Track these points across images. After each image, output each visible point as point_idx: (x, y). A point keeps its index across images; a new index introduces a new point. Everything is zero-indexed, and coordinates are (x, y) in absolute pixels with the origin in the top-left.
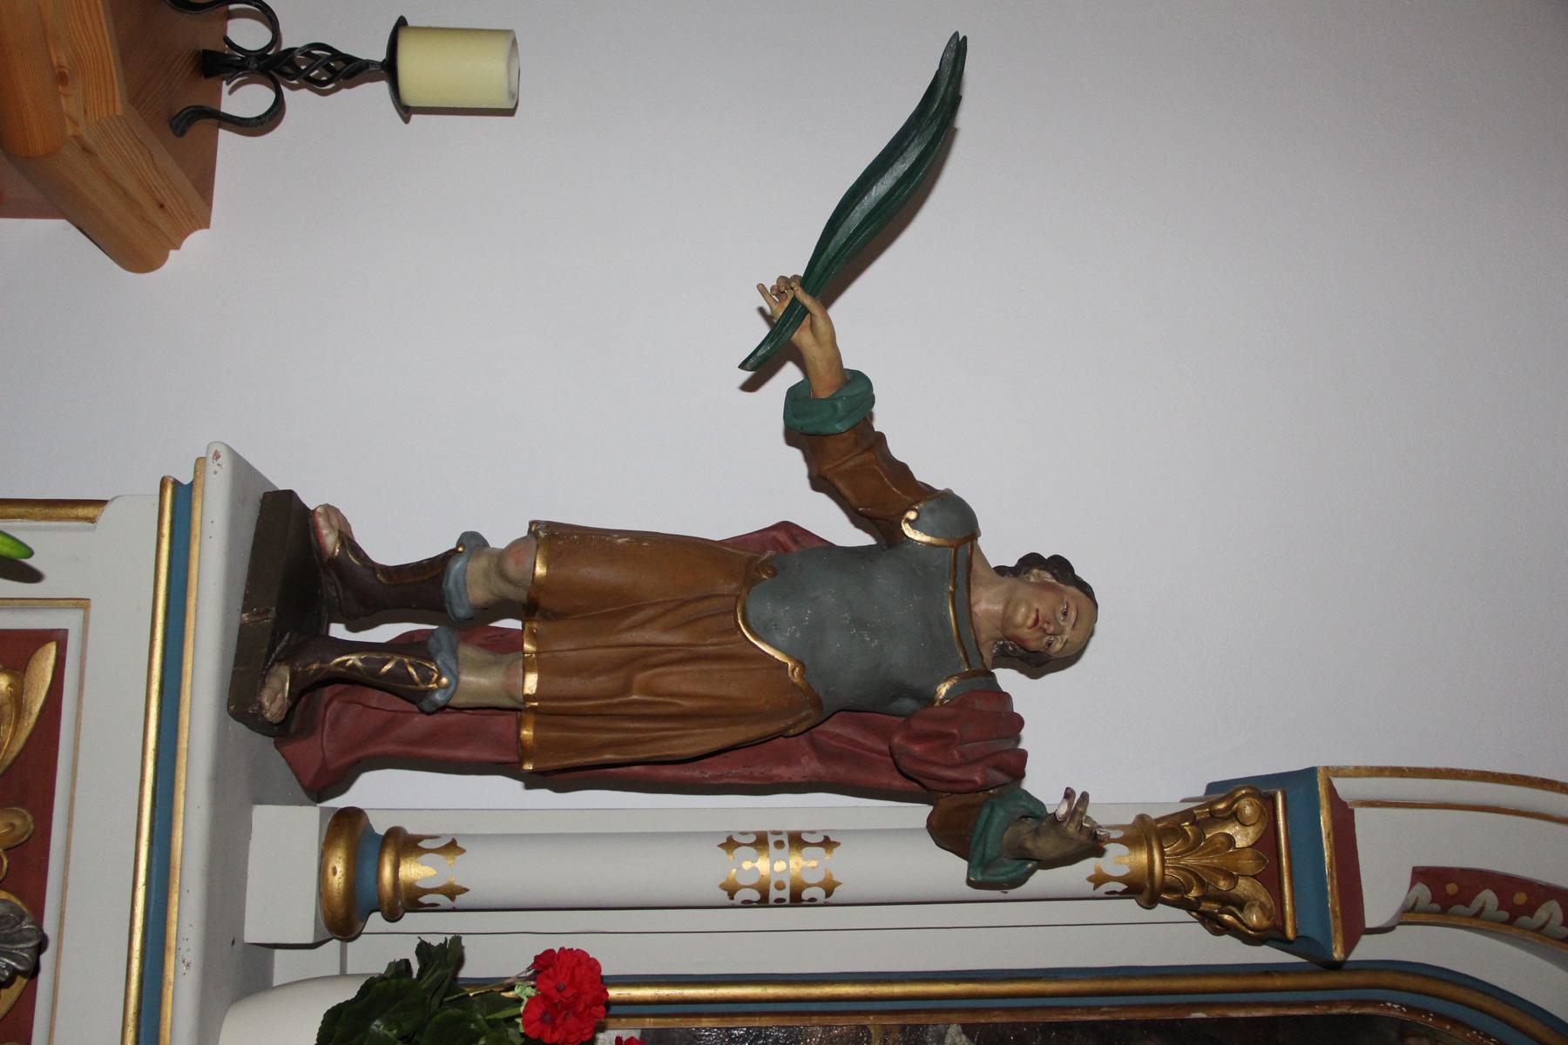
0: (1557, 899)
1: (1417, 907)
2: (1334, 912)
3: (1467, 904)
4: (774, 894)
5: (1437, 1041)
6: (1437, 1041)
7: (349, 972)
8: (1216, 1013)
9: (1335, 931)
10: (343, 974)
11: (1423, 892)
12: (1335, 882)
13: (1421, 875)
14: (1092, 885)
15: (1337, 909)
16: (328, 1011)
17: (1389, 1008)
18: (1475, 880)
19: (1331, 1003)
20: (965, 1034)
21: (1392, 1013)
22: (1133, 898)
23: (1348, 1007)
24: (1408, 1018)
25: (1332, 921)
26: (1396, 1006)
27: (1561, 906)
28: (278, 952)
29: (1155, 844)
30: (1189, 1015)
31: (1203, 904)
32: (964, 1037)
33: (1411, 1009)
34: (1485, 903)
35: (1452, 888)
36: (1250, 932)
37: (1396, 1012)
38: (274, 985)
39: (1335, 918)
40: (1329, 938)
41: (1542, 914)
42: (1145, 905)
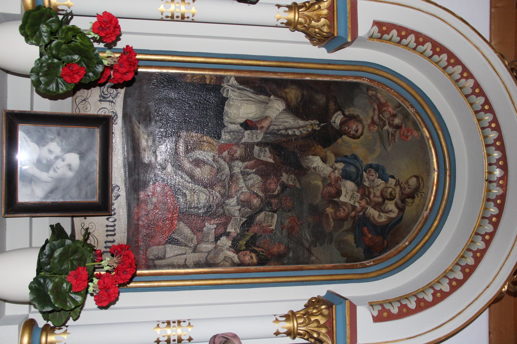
0: (414, 34)
1: (373, 36)
2: (349, 28)
3: (388, 34)
4: (176, 324)
5: (377, 92)
6: (377, 92)
7: (33, 246)
8: (313, 78)
9: (349, 33)
10: (31, 246)
11: (376, 29)
12: (350, 19)
13: (376, 23)
14: (275, 335)
15: (350, 27)
16: (20, 26)
17: (365, 80)
18: (391, 26)
19: (348, 77)
20: (236, 80)
21: (365, 81)
22: (288, 28)
23: (352, 79)
24: (369, 84)
25: (348, 30)
26: (366, 79)
27: (415, 36)
28: (7, 304)
29: (297, 11)
30: (305, 78)
31: (310, 29)
32: (236, 81)
33: (371, 80)
34: (393, 34)
35: (384, 28)
36: (325, 34)
37: (366, 82)
38: (7, 250)
39: (349, 29)
40: (347, 35)
41: (409, 38)
42: (294, 30)
